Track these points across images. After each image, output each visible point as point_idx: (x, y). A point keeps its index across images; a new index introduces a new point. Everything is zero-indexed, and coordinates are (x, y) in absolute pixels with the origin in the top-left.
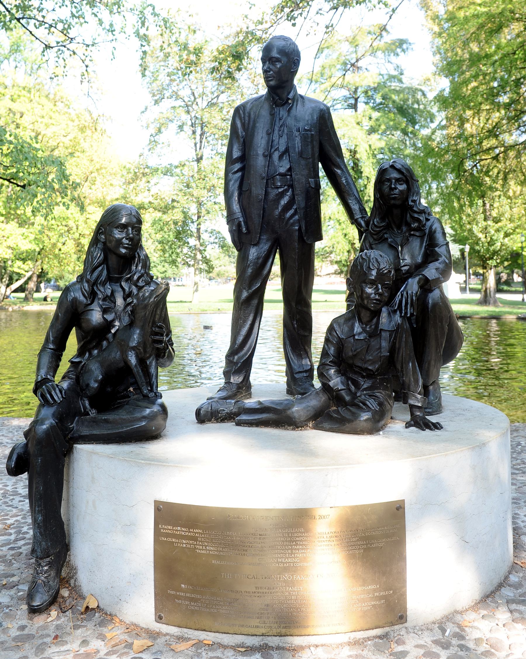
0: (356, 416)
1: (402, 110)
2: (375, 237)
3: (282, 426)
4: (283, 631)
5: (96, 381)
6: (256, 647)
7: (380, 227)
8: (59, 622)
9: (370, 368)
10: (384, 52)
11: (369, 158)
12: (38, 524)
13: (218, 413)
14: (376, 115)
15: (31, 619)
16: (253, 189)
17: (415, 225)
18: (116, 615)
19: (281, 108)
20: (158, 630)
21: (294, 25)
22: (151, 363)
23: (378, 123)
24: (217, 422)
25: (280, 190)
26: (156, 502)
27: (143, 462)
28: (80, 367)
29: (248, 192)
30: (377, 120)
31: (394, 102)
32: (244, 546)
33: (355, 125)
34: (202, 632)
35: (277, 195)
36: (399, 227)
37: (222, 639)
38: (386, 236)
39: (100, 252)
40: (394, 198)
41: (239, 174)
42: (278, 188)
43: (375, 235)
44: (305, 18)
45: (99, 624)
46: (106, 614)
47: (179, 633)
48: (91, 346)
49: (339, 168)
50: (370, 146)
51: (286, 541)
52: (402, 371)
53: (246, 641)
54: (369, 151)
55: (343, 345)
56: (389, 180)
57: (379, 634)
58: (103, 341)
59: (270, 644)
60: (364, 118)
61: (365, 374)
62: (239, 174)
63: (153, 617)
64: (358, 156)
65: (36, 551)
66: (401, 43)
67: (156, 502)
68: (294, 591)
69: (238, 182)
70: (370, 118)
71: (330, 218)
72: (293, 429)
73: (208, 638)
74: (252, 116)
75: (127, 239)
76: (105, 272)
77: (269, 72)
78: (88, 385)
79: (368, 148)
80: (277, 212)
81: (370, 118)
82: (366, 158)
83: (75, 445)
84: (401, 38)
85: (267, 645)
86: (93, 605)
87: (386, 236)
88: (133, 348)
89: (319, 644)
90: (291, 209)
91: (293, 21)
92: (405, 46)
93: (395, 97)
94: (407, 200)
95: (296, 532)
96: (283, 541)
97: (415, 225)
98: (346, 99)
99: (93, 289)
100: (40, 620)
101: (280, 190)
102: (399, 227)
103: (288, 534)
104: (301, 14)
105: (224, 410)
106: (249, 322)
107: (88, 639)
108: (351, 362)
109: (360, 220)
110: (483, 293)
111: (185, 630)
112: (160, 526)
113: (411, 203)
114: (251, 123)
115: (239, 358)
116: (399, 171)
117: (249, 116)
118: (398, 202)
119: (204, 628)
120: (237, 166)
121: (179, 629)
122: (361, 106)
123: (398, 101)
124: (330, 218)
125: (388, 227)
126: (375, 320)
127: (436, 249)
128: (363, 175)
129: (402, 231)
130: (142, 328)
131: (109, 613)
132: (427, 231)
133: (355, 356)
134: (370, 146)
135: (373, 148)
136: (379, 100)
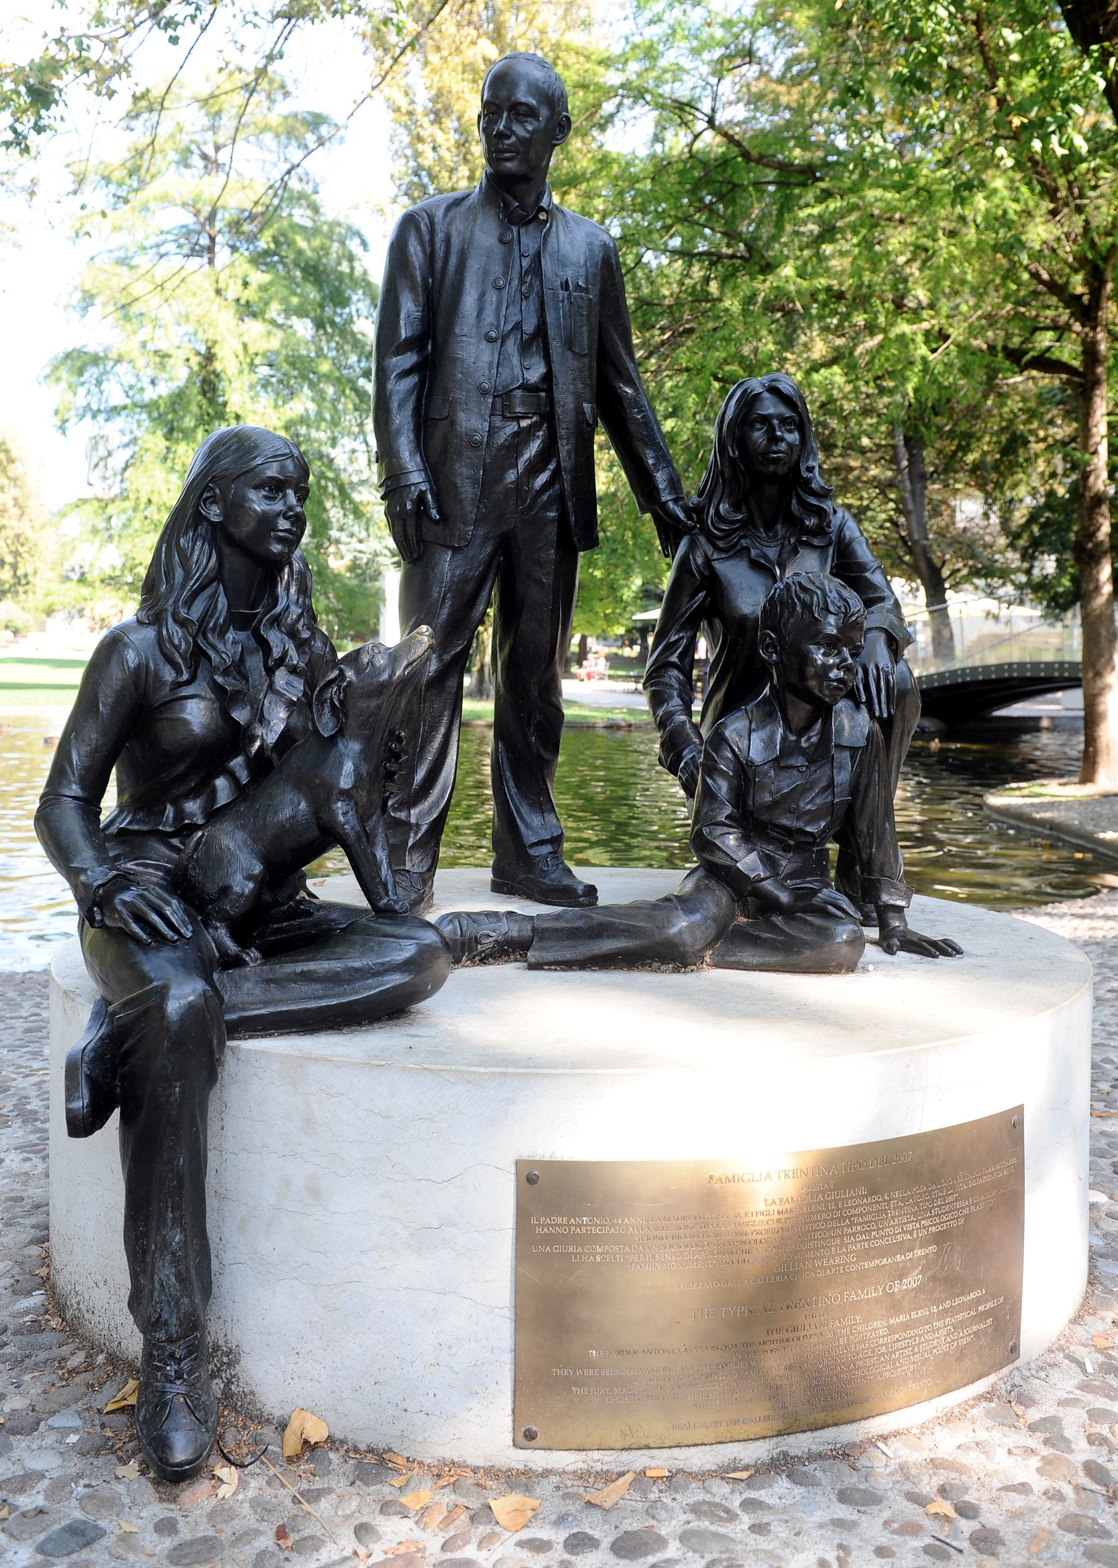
0: (826, 935)
1: (314, 272)
2: (721, 544)
3: (643, 965)
4: (821, 1417)
5: (249, 878)
6: (763, 1464)
7: (734, 522)
8: (251, 1493)
9: (808, 829)
10: (277, 136)
11: (241, 372)
12: (173, 1254)
13: (477, 941)
14: (259, 277)
15: (174, 1500)
16: (462, 416)
17: (811, 522)
18: (390, 1450)
19: (523, 230)
20: (521, 1467)
21: (174, 40)
22: (374, 828)
23: (265, 296)
24: (474, 964)
25: (524, 423)
26: (519, 1164)
27: (482, 1070)
28: (192, 844)
29: (447, 422)
30: (263, 288)
31: (300, 252)
32: (744, 1243)
33: (213, 294)
34: (640, 1452)
35: (516, 434)
36: (769, 527)
37: (687, 1459)
38: (744, 542)
39: (206, 547)
40: (776, 461)
41: (413, 380)
42: (517, 419)
43: (720, 538)
44: (203, 29)
45: (358, 1477)
46: (356, 1450)
47: (580, 1465)
48: (182, 789)
49: (630, 382)
50: (245, 346)
51: (832, 1219)
52: (870, 835)
53: (741, 1456)
54: (242, 358)
55: (747, 780)
56: (766, 419)
57: (981, 1391)
58: (218, 777)
59: (793, 1452)
60: (231, 282)
61: (792, 843)
62: (413, 380)
63: (508, 1438)
64: (217, 366)
65: (166, 1323)
66: (316, 121)
67: (519, 1164)
68: (844, 1327)
69: (413, 397)
70: (246, 284)
71: (150, 501)
72: (676, 970)
73: (653, 1464)
74: (455, 241)
75: (286, 518)
76: (222, 602)
77: (509, 138)
78: (225, 890)
79: (240, 351)
80: (511, 476)
81: (246, 284)
82: (236, 372)
83: (229, 1043)
84: (317, 110)
85: (785, 1454)
86: (317, 1433)
87: (744, 542)
88: (346, 794)
89: (886, 1432)
90: (543, 470)
91: (170, 32)
92: (324, 130)
93: (302, 244)
94: (797, 465)
95: (852, 1198)
96: (825, 1221)
97: (811, 522)
98: (188, 233)
99: (195, 643)
100: (198, 1497)
101: (524, 423)
102: (769, 527)
103: (836, 1201)
104: (193, 18)
105: (489, 936)
106: (442, 730)
107: (364, 1520)
108: (765, 817)
109: (671, 504)
110: (475, 675)
111: (596, 1455)
112: (534, 1221)
113: (805, 474)
114: (453, 261)
115: (421, 815)
116: (786, 399)
117: (448, 240)
118: (782, 470)
119: (644, 1442)
120: (409, 359)
121: (581, 1456)
122: (222, 254)
123: (309, 254)
124: (150, 501)
125: (747, 525)
126: (818, 726)
127: (867, 574)
128: (228, 410)
129: (776, 534)
130: (367, 742)
131: (363, 1447)
132: (833, 537)
133: (775, 804)
134: (245, 346)
135: (251, 351)
136: (264, 242)
